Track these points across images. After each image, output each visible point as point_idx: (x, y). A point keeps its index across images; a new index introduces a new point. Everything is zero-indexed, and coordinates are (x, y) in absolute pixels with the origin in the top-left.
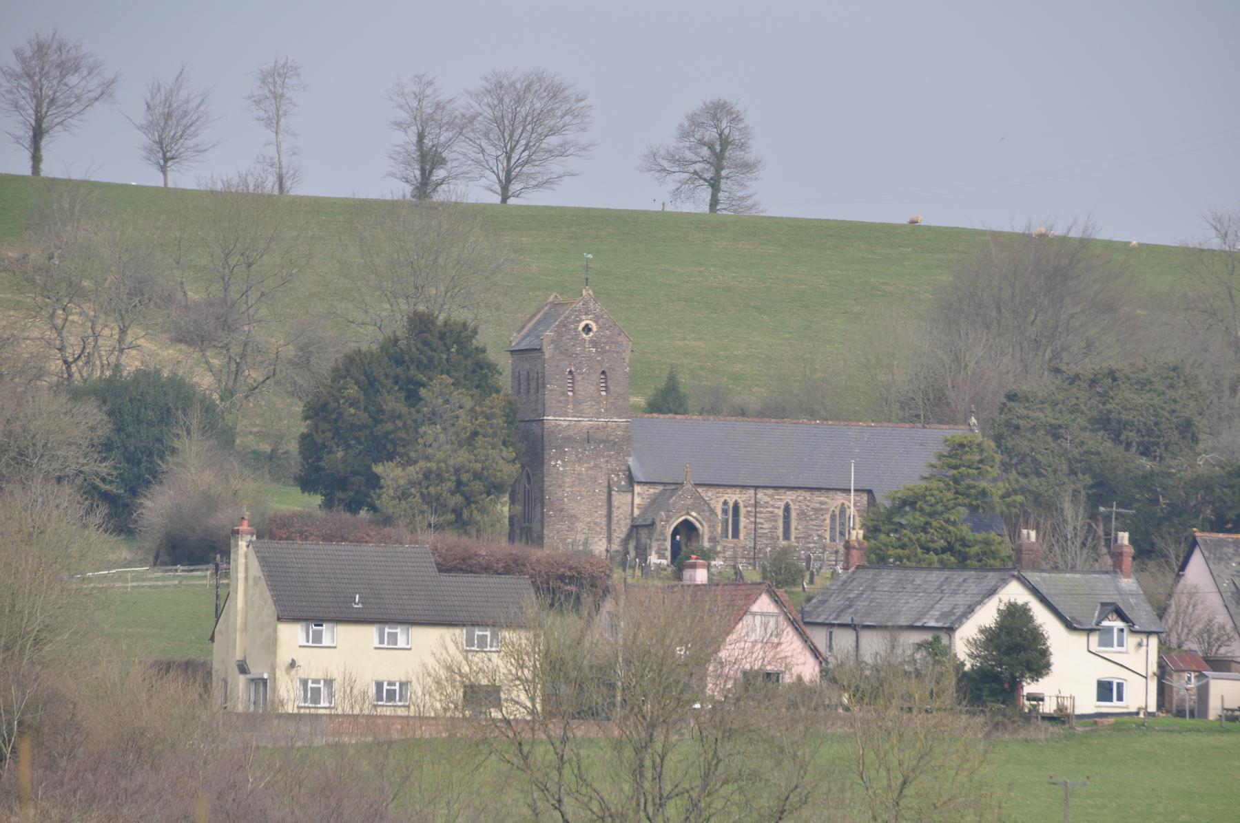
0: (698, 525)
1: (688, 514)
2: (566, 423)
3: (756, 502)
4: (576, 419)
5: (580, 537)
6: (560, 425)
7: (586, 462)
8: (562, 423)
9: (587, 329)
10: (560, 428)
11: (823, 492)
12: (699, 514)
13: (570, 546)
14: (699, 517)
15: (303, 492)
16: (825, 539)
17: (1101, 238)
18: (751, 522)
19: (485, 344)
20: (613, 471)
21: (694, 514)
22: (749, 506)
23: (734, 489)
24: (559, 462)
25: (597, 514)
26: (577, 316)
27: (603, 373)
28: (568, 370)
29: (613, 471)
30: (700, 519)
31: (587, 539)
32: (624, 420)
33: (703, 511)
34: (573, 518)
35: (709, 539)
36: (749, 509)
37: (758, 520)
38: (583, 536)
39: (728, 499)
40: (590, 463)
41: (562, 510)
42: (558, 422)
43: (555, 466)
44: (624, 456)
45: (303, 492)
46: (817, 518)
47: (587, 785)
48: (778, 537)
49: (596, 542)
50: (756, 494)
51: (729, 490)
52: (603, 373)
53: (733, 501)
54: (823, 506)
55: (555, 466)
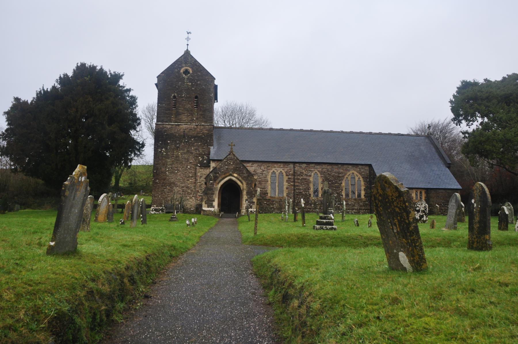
0: (239, 183)
1: (231, 175)
2: (170, 126)
3: (294, 172)
4: (176, 124)
5: (177, 196)
6: (165, 127)
7: (182, 149)
8: (167, 126)
9: (186, 72)
10: (165, 129)
11: (340, 166)
12: (239, 175)
13: (170, 202)
14: (239, 177)
15: (458, 88)
16: (342, 195)
17: (153, 158)
18: (292, 185)
19: (102, 66)
20: (200, 155)
21: (235, 175)
22: (290, 175)
23: (279, 164)
24: (163, 149)
25: (188, 182)
26: (180, 65)
27: (196, 97)
28: (173, 95)
29: (200, 155)
30: (240, 178)
31: (182, 198)
32: (209, 124)
33: (243, 173)
34: (172, 184)
35: (247, 193)
36: (290, 177)
37: (297, 184)
38: (179, 196)
39: (275, 171)
40: (136, 333)
41: (164, 179)
42: (164, 126)
43: (161, 152)
44: (208, 146)
45: (458, 88)
46: (336, 182)
47: (195, 178)
48: (310, 195)
49: (188, 200)
50: (294, 167)
51: (275, 165)
52: (196, 97)
53: (279, 171)
54: (340, 175)
55: (161, 152)
